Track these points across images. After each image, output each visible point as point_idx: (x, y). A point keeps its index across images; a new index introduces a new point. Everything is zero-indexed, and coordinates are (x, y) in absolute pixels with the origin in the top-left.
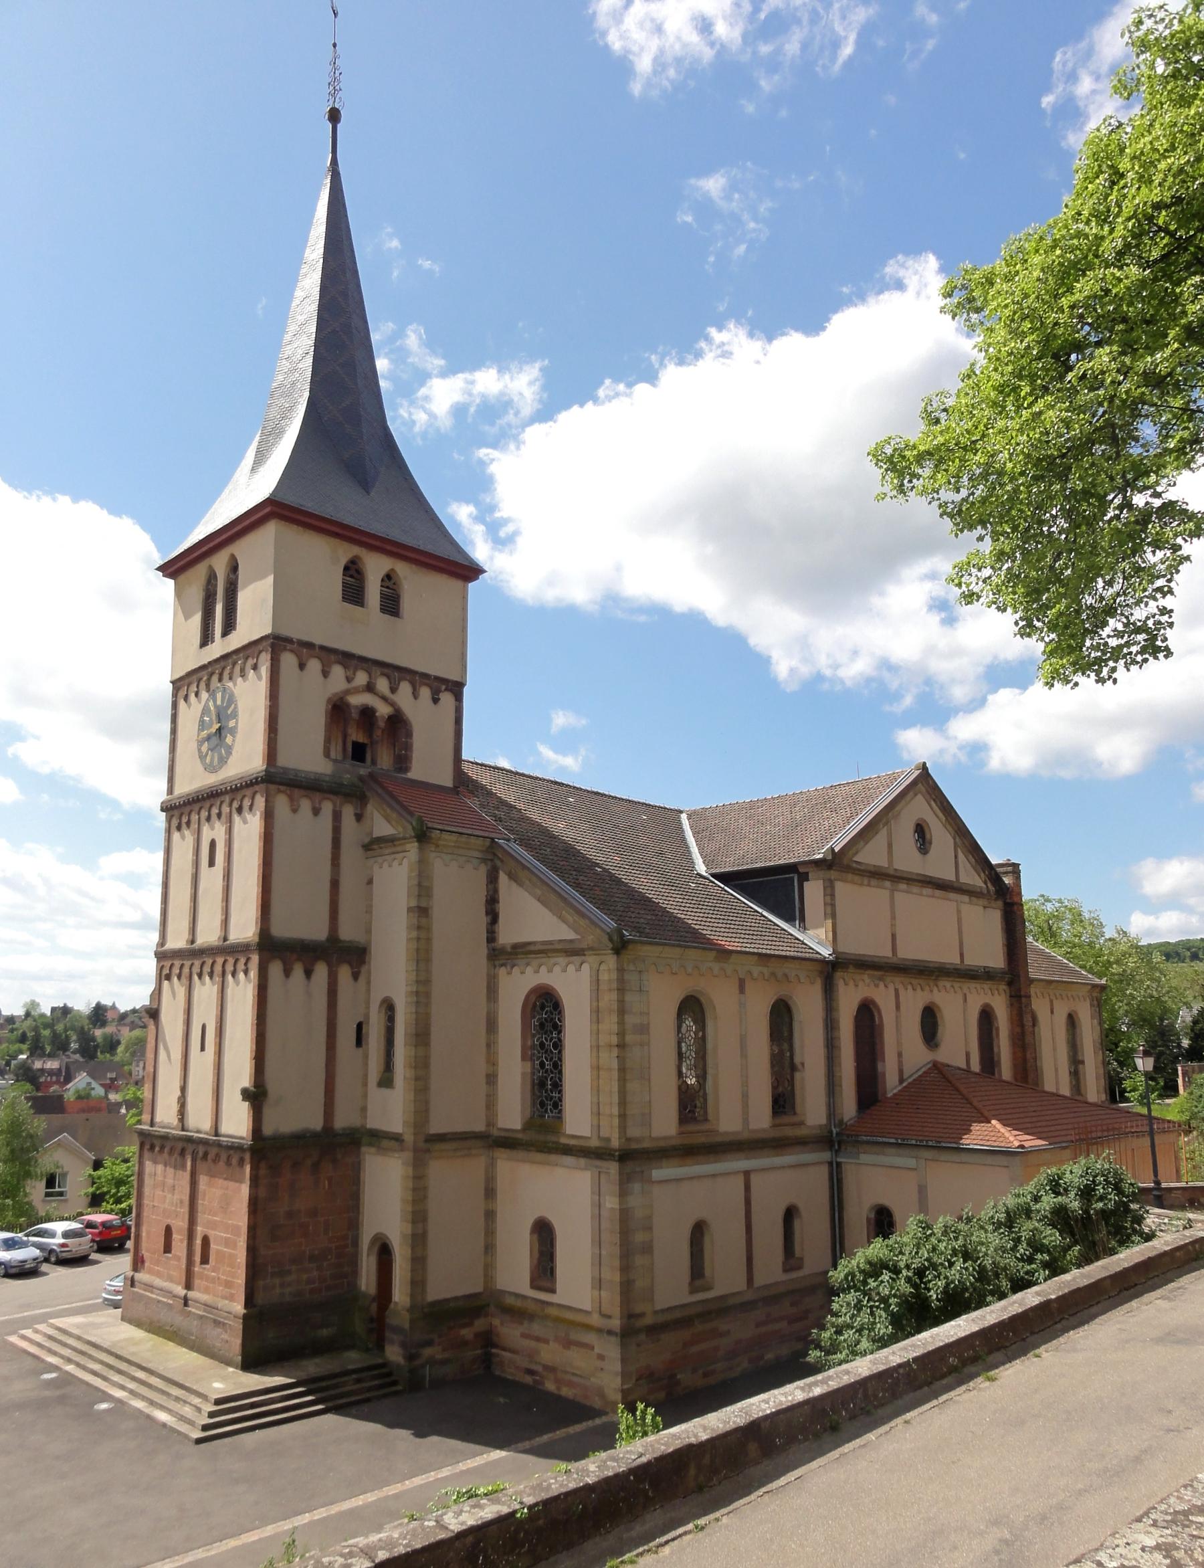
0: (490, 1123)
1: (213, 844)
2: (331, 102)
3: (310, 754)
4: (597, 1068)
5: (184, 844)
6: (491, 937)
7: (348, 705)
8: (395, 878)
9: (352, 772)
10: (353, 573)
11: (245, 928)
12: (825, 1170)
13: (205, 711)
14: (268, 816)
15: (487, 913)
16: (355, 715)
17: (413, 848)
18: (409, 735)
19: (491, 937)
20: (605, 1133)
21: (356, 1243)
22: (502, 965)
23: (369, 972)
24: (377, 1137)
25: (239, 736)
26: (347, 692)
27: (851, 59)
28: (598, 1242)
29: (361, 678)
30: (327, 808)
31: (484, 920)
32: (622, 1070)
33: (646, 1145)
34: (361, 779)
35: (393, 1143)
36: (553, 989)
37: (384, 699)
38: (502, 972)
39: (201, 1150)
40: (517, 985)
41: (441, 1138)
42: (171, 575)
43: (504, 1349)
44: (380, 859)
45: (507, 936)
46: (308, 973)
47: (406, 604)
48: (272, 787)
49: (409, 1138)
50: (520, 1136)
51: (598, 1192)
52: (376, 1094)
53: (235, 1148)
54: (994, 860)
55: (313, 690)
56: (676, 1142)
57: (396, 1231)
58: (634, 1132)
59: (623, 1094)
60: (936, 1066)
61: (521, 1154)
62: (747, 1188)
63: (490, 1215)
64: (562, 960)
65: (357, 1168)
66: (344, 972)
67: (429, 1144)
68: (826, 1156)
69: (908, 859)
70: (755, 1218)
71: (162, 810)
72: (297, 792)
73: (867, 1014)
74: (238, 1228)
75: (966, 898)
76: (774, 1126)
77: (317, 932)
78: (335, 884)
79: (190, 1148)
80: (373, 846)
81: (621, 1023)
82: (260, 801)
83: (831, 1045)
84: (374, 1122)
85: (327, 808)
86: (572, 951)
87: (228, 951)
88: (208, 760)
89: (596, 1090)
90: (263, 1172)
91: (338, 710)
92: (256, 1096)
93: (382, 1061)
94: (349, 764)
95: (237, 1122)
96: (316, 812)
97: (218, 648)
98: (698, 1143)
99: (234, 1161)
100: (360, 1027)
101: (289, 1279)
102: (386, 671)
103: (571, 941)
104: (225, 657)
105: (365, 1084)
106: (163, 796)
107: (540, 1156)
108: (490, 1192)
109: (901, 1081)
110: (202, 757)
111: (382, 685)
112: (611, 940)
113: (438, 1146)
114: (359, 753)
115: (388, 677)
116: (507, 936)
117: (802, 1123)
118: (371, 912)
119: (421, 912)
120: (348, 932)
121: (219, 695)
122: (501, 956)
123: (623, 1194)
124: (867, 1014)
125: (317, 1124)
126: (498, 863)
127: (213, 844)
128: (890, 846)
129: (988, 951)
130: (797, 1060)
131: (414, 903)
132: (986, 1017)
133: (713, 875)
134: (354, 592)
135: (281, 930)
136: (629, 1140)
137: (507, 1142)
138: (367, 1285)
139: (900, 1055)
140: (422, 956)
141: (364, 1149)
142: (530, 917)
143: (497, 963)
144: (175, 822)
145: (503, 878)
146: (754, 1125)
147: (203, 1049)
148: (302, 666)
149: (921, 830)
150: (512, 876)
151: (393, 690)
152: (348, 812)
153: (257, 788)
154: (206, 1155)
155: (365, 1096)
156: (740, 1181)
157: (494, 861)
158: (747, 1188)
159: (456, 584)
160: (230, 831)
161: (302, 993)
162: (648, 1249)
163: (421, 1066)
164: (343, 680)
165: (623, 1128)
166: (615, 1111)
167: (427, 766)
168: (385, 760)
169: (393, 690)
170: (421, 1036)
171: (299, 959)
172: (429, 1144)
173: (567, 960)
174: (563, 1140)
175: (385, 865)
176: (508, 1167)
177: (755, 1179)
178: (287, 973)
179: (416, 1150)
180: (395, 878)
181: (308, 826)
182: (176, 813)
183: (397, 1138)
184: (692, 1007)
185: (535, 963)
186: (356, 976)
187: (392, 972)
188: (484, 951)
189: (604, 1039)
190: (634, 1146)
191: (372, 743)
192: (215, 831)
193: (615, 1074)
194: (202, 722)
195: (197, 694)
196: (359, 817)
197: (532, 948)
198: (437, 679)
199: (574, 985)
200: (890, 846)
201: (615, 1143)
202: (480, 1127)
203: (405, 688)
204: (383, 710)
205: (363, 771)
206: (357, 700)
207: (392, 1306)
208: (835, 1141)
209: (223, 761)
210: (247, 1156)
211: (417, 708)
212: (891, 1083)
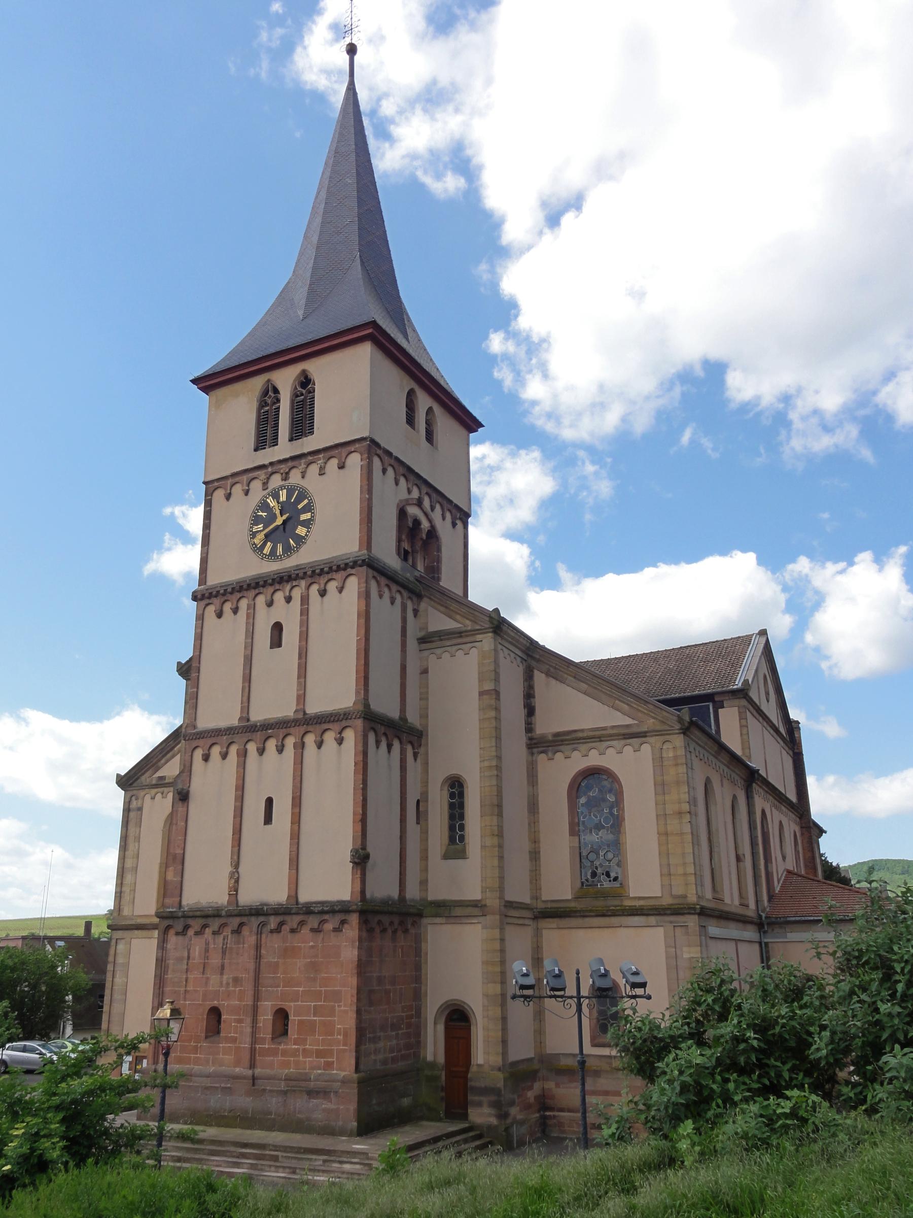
0: (536, 898)
1: (278, 628)
4: (664, 835)
6: (529, 728)
14: (366, 596)
18: (439, 549)
19: (529, 728)
22: (542, 752)
23: (427, 754)
24: (446, 910)
25: (315, 528)
29: (415, 494)
35: (476, 911)
37: (426, 514)
39: (273, 922)
42: (206, 390)
43: (561, 1110)
44: (439, 651)
45: (545, 727)
46: (389, 747)
47: (232, 499)
49: (493, 902)
50: (573, 905)
51: (672, 945)
52: (438, 867)
53: (338, 910)
65: (418, 940)
66: (409, 749)
74: (336, 996)
78: (403, 668)
80: (425, 640)
87: (309, 724)
89: (665, 854)
92: (361, 860)
96: (393, 602)
97: (284, 449)
101: (381, 1044)
103: (628, 726)
106: (195, 586)
118: (427, 699)
120: (413, 718)
121: (283, 496)
122: (538, 745)
126: (534, 663)
127: (278, 628)
133: (659, 701)
138: (435, 1055)
143: (535, 750)
147: (268, 819)
148: (384, 471)
151: (433, 509)
154: (278, 930)
159: (462, 431)
160: (305, 613)
164: (406, 491)
170: (496, 807)
173: (623, 742)
174: (627, 903)
176: (554, 936)
178: (378, 743)
183: (478, 906)
185: (583, 748)
188: (523, 739)
189: (670, 808)
191: (413, 551)
192: (287, 613)
196: (416, 612)
197: (580, 735)
201: (692, 899)
204: (425, 524)
207: (473, 1069)
210: (354, 919)
211: (444, 527)
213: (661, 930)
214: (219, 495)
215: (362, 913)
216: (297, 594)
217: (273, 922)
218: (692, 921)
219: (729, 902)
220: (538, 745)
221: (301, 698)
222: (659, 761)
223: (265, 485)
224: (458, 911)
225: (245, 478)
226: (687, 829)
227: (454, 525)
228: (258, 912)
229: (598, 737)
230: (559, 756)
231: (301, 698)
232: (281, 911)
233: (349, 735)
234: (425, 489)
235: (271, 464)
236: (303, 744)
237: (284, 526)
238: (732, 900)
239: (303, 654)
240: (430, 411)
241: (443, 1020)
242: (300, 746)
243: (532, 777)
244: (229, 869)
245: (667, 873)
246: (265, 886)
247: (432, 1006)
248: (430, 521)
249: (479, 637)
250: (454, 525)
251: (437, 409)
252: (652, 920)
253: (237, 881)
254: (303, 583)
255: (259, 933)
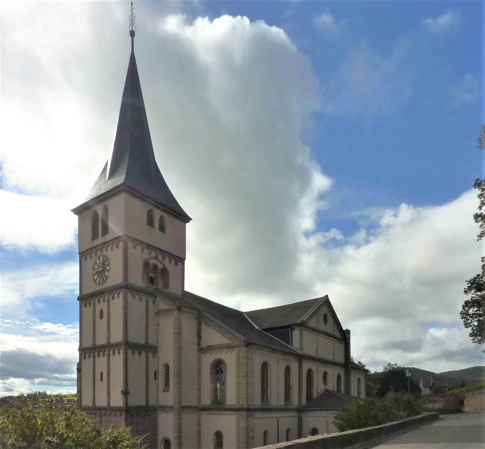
0: (199, 404)
1: (102, 311)
2: (131, 28)
3: (138, 279)
5: (89, 310)
6: (199, 344)
7: (149, 263)
8: (168, 324)
9: (151, 288)
10: (150, 215)
11: (117, 337)
12: (297, 418)
13: (95, 263)
14: (125, 299)
15: (198, 336)
16: (152, 267)
17: (176, 313)
18: (168, 275)
19: (199, 344)
20: (240, 403)
21: (156, 441)
24: (163, 408)
26: (149, 259)
27: (289, 33)
28: (238, 435)
30: (144, 299)
31: (196, 339)
32: (247, 383)
33: (253, 407)
34: (154, 289)
36: (211, 365)
37: (160, 262)
38: (203, 355)
40: (208, 360)
41: (185, 407)
44: (162, 317)
45: (205, 343)
46: (140, 354)
48: (127, 290)
49: (176, 407)
50: (210, 407)
51: (238, 421)
53: (117, 409)
54: (344, 329)
55: (138, 256)
56: (261, 407)
57: (171, 435)
58: (250, 403)
59: (247, 390)
60: (326, 390)
61: (210, 412)
62: (278, 422)
63: (199, 432)
64: (226, 350)
65: (156, 417)
66: (150, 355)
67: (182, 409)
68: (297, 414)
69: (321, 326)
70: (280, 431)
71: (78, 300)
72: (134, 292)
73: (310, 372)
75: (336, 340)
76: (285, 405)
77: (142, 341)
79: (99, 412)
80: (159, 313)
81: (247, 369)
82: (121, 294)
83: (300, 381)
84: (162, 403)
85: (144, 299)
86: (230, 347)
88: (97, 281)
90: (129, 417)
91: (146, 264)
92: (126, 393)
93: (164, 383)
94: (150, 285)
95: (118, 401)
96: (141, 300)
97: (100, 240)
98: (266, 409)
99: (118, 414)
100: (155, 373)
102: (162, 252)
103: (229, 344)
104: (104, 243)
105: (158, 391)
107: (218, 412)
108: (199, 425)
109: (317, 393)
110: (95, 281)
111: (160, 257)
112: (244, 342)
113: (185, 409)
114: (152, 281)
115: (162, 254)
116: (205, 343)
117: (292, 405)
119: (178, 334)
120: (151, 342)
121: (101, 258)
122: (202, 350)
123: (247, 421)
124: (310, 372)
125: (144, 404)
127: (102, 311)
128: (317, 321)
129: (341, 359)
130: (291, 385)
131: (176, 331)
132: (339, 376)
133: (262, 329)
134: (150, 223)
135: (132, 339)
136: (249, 405)
137: (205, 409)
139: (317, 386)
140: (179, 349)
141: (158, 412)
142: (213, 336)
144: (83, 304)
145: (203, 325)
146: (280, 404)
147: (102, 380)
148: (135, 248)
149: (325, 317)
150: (206, 324)
151: (163, 259)
152: (151, 300)
153: (121, 290)
154: (105, 414)
155: (158, 395)
156: (276, 420)
157: (200, 319)
158: (278, 422)
159: (181, 223)
160: (109, 306)
161: (137, 361)
162: (253, 438)
163: (179, 385)
165: (247, 401)
166: (245, 396)
167: (173, 288)
168: (160, 285)
169: (163, 259)
170: (179, 375)
171: (137, 350)
172: (182, 409)
174: (226, 407)
175: (164, 319)
176: (204, 416)
177: (280, 420)
178: (133, 353)
179: (179, 411)
180: (168, 324)
181: (138, 305)
182: (84, 301)
183: (172, 407)
184: (265, 366)
186: (154, 356)
187: (167, 354)
188: (196, 348)
190: (250, 407)
192: (103, 305)
193: (245, 385)
194: (94, 268)
195: (91, 258)
196: (154, 303)
198: (177, 257)
199: (230, 358)
200: (317, 321)
202: (196, 404)
203: (167, 259)
204: (160, 266)
205: (155, 287)
206: (153, 262)
208: (300, 410)
209: (104, 282)
210: (124, 412)
211: (170, 266)
212: (315, 395)
213: (235, 416)
214: (83, 258)
215: (126, 411)
216: (106, 298)
217: (104, 412)
218: (244, 413)
219: (356, 396)
220: (202, 350)
221: (109, 338)
222: (238, 356)
223: (96, 256)
224: (167, 409)
225: (90, 252)
226: (245, 382)
227: (176, 264)
228: (100, 409)
229: (220, 348)
230: (208, 354)
231: (109, 338)
232: (105, 409)
233: (121, 351)
234: (158, 252)
235: (97, 246)
236: (109, 354)
237: (102, 272)
238: (359, 393)
239: (109, 321)
240: (161, 218)
241: (163, 442)
242: (109, 354)
243: (199, 362)
244: (92, 395)
245: (238, 397)
246: (102, 402)
247: (160, 438)
248: (163, 264)
249: (174, 312)
250: (176, 264)
251: (166, 216)
252: (233, 412)
253: (95, 399)
254: (108, 294)
255: (101, 416)
